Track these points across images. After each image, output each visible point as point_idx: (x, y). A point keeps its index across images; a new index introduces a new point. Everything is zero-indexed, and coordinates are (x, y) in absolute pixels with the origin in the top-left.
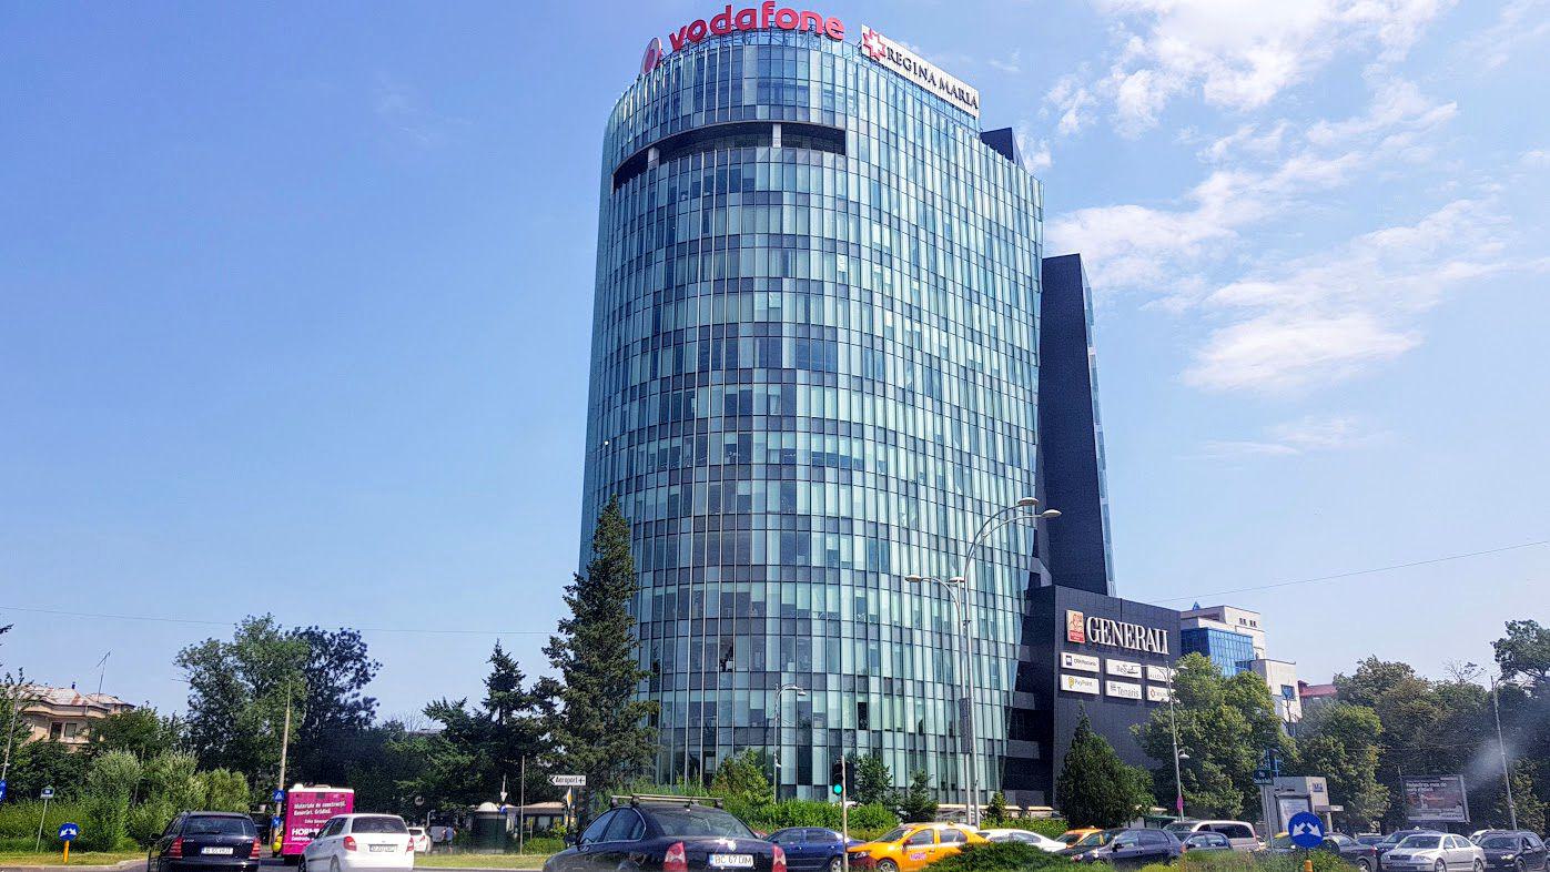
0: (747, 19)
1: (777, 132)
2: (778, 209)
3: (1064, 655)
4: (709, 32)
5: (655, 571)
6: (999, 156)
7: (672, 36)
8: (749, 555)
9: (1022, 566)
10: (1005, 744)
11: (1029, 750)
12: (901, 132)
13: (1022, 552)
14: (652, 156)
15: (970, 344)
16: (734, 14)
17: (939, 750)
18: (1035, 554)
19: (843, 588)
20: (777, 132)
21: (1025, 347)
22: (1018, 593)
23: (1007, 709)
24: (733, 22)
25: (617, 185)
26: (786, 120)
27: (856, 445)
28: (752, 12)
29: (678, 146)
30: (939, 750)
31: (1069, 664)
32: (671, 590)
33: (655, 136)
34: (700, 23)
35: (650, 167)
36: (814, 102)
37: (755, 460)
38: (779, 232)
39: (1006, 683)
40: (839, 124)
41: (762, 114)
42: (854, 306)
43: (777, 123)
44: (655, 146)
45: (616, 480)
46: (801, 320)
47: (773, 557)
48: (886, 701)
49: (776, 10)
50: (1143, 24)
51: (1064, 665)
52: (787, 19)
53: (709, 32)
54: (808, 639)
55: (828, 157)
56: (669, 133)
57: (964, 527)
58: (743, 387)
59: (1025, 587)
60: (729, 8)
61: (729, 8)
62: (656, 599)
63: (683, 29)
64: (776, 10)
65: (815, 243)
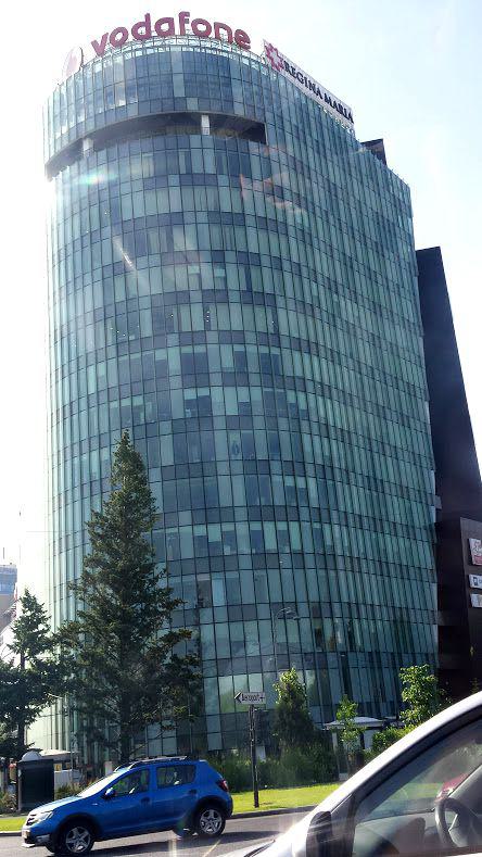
0: (165, 27)
1: (205, 123)
2: (225, 306)
3: (471, 576)
4: (131, 38)
7: (94, 44)
12: (307, 131)
14: (86, 146)
15: (320, 399)
16: (153, 24)
20: (205, 123)
24: (153, 28)
27: (302, 396)
28: (170, 21)
31: (476, 584)
34: (122, 30)
37: (148, 313)
38: (202, 171)
40: (259, 119)
41: (192, 105)
42: (288, 276)
46: (244, 288)
47: (240, 500)
48: (299, 573)
49: (191, 19)
50: (31, 839)
51: (473, 586)
52: (202, 28)
53: (131, 38)
57: (388, 470)
60: (148, 17)
61: (148, 17)
63: (105, 37)
64: (191, 19)
65: (250, 221)
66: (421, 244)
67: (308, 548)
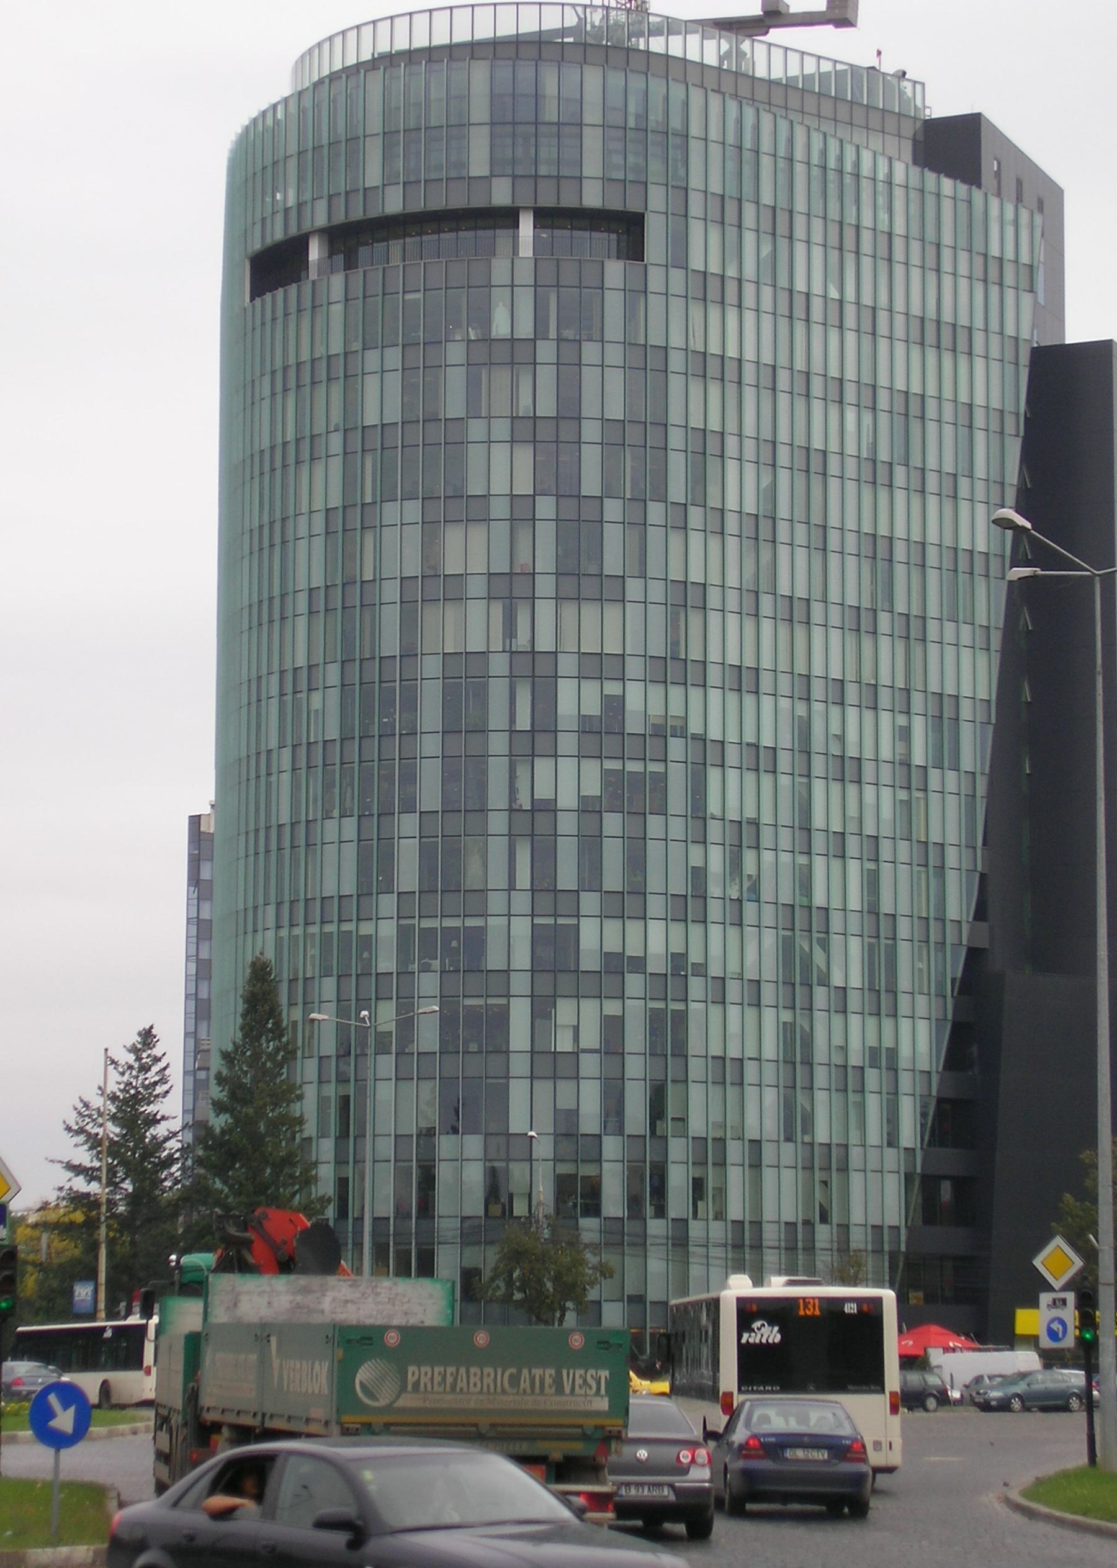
5: (339, 977)
6: (947, 184)
8: (464, 480)
9: (950, 939)
10: (903, 1231)
11: (950, 1239)
13: (953, 911)
14: (315, 252)
17: (964, 867)
18: (981, 913)
19: (691, 533)
20: (526, 226)
21: (981, 547)
22: (941, 984)
23: (909, 1178)
25: (257, 292)
26: (547, 201)
29: (350, 239)
30: (964, 867)
32: (346, 927)
33: (321, 221)
35: (313, 274)
36: (592, 167)
39: (909, 1133)
40: (634, 206)
41: (501, 195)
43: (526, 208)
44: (322, 231)
45: (263, 748)
54: (573, 921)
55: (615, 271)
56: (340, 218)
57: (838, 886)
58: (471, 922)
59: (955, 968)
62: (326, 938)
66: (1078, 331)
67: (855, 981)
